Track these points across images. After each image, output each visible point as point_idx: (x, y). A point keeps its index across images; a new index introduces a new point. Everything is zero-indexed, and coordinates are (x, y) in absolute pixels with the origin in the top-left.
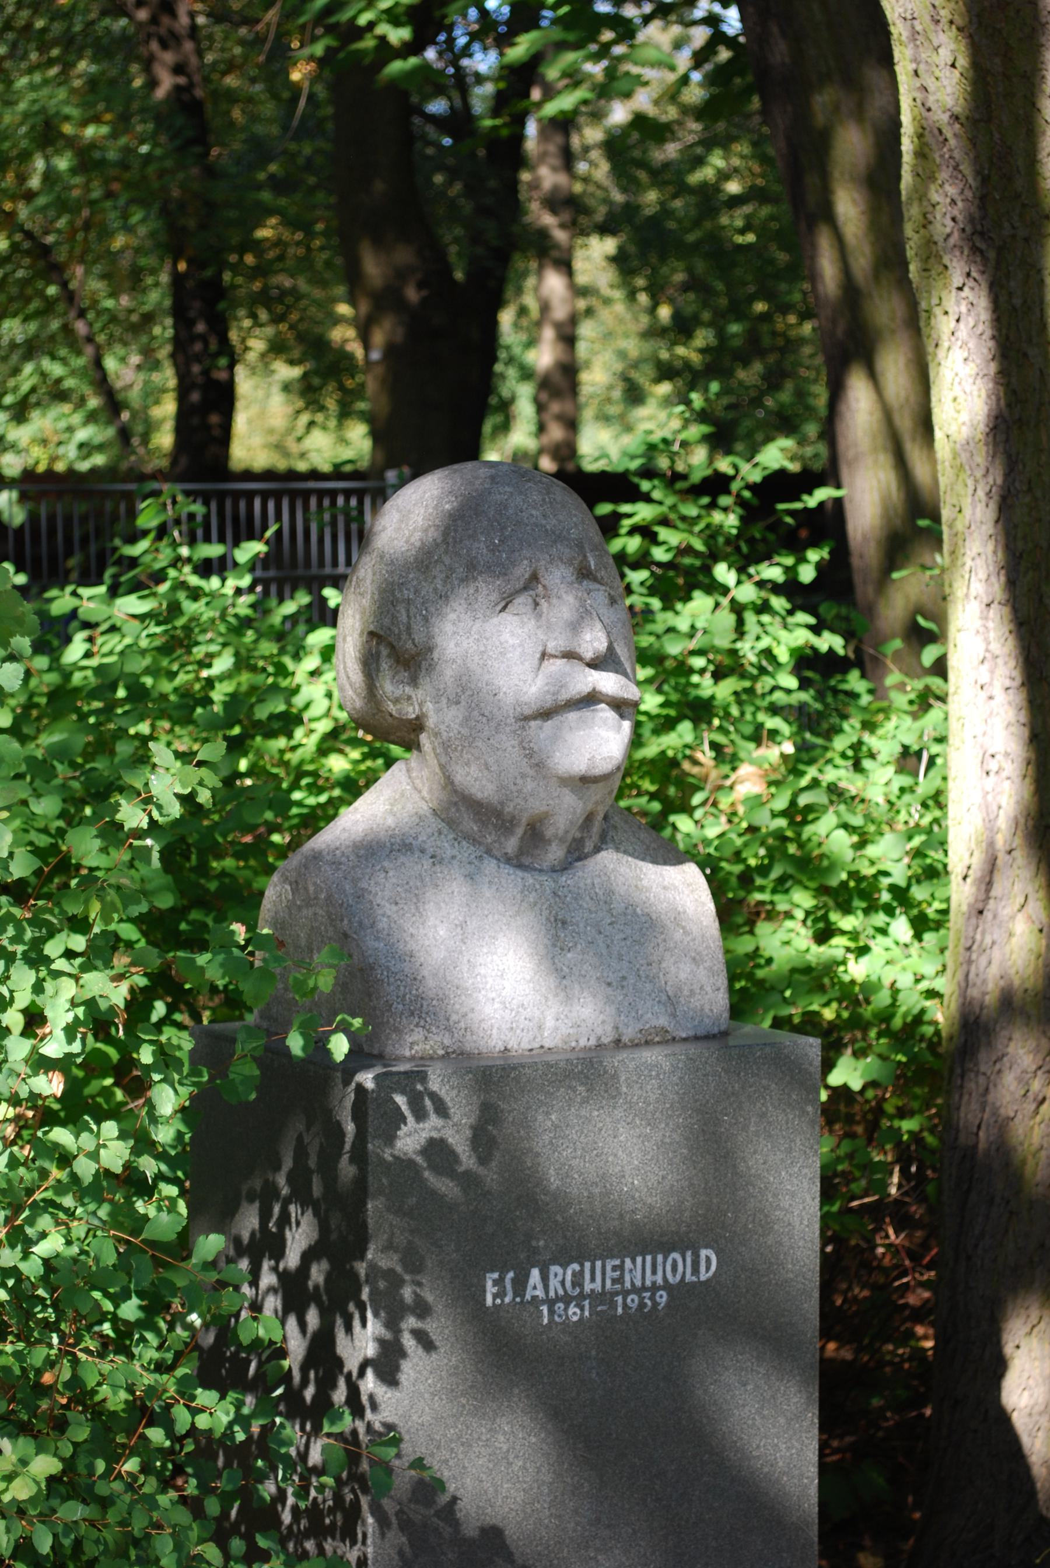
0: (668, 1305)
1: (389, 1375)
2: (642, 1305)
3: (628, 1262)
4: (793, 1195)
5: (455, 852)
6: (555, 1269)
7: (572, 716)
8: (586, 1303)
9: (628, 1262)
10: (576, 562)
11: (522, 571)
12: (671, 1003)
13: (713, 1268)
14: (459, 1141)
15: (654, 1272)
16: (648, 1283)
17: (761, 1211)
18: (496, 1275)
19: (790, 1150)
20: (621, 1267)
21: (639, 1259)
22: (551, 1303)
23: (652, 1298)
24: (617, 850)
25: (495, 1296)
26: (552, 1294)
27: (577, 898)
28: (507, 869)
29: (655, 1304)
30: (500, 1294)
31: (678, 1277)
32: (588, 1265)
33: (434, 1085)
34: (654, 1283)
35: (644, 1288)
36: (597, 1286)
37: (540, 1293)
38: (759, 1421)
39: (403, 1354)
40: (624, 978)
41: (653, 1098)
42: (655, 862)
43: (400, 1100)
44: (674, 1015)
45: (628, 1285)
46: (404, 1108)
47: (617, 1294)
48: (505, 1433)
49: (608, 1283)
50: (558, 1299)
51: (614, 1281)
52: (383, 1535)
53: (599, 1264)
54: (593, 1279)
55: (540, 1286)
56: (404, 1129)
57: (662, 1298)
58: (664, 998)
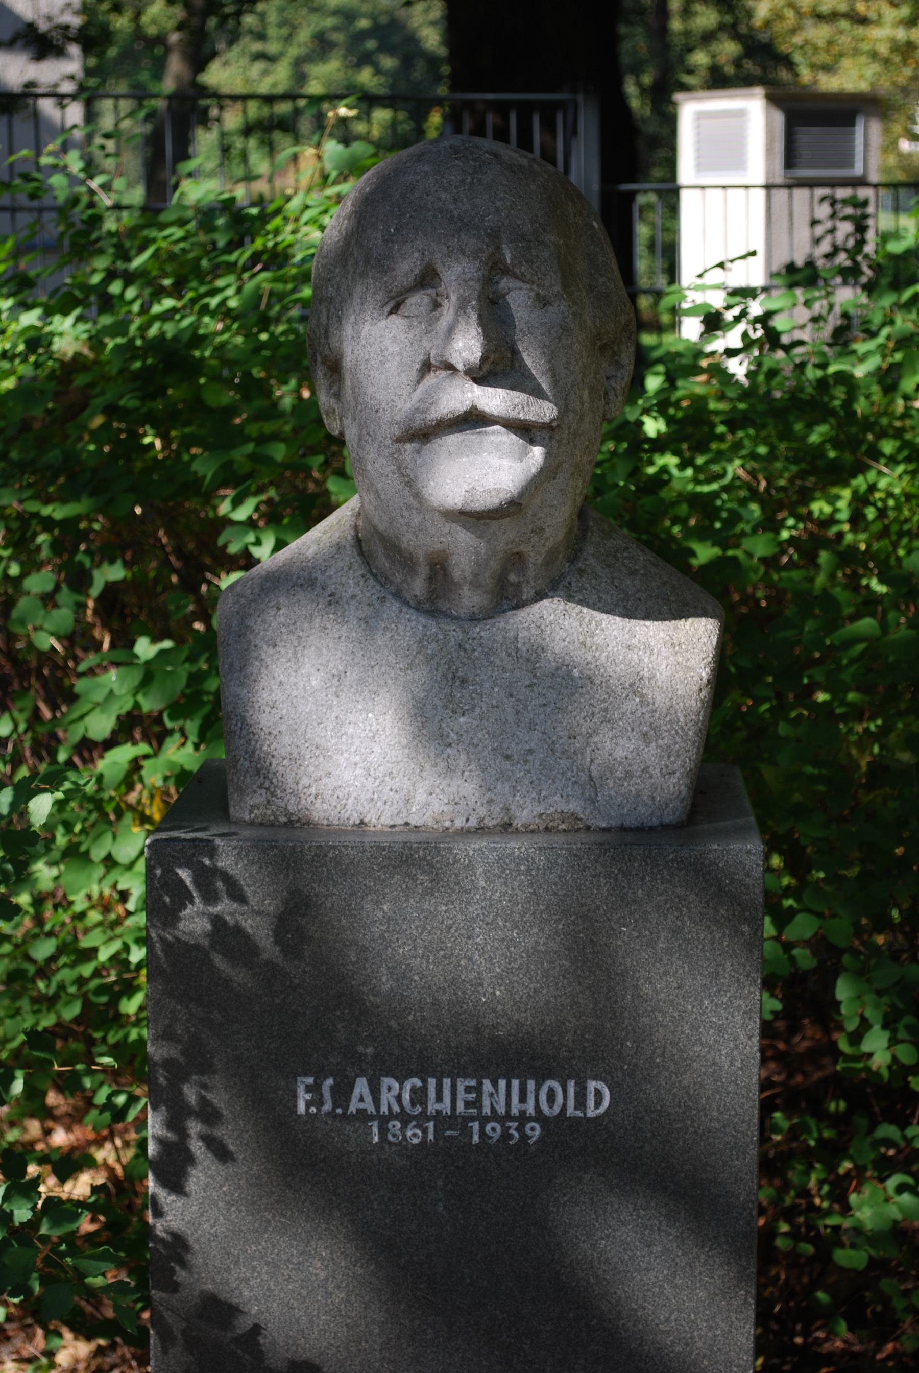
0: (541, 1139)
1: (174, 1182)
2: (506, 1136)
3: (487, 1085)
4: (720, 1030)
5: (357, 591)
6: (387, 1081)
7: (452, 440)
8: (431, 1125)
9: (487, 1085)
10: (484, 256)
11: (407, 267)
12: (592, 786)
13: (606, 1103)
14: (256, 926)
15: (523, 1099)
16: (515, 1111)
17: (674, 1044)
18: (310, 1080)
19: (716, 976)
20: (478, 1089)
21: (502, 1083)
22: (384, 1120)
23: (520, 1129)
24: (569, 598)
25: (308, 1104)
26: (384, 1109)
27: (489, 652)
28: (412, 614)
29: (524, 1137)
30: (318, 1102)
31: (557, 1109)
32: (432, 1082)
33: (225, 862)
34: (523, 1113)
35: (508, 1116)
36: (446, 1106)
37: (369, 1107)
38: (668, 1290)
39: (190, 1159)
40: (531, 751)
41: (522, 896)
42: (629, 614)
43: (184, 874)
44: (593, 801)
45: (487, 1110)
46: (188, 881)
47: (473, 1119)
48: (322, 1259)
49: (460, 1106)
50: (391, 1116)
51: (467, 1104)
52: (165, 1351)
53: (447, 1082)
54: (439, 1099)
55: (368, 1099)
56: (189, 911)
57: (535, 1131)
58: (584, 778)
